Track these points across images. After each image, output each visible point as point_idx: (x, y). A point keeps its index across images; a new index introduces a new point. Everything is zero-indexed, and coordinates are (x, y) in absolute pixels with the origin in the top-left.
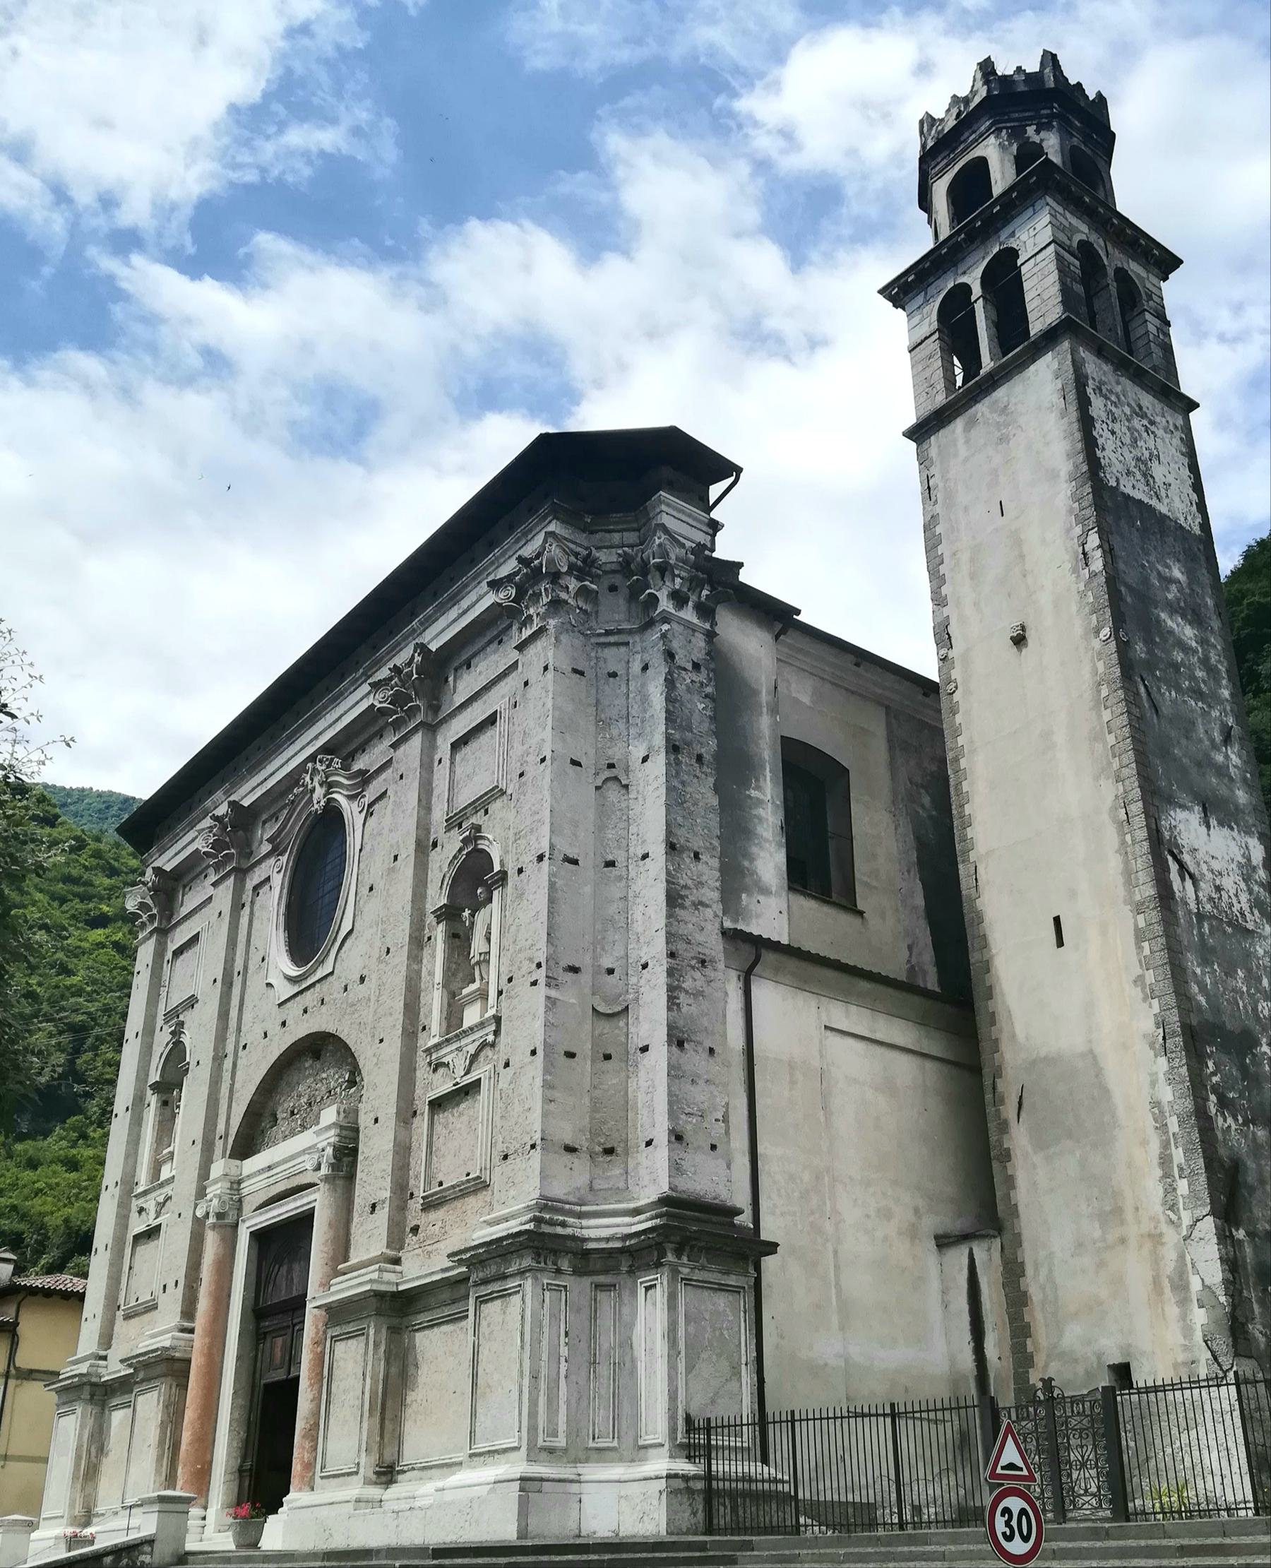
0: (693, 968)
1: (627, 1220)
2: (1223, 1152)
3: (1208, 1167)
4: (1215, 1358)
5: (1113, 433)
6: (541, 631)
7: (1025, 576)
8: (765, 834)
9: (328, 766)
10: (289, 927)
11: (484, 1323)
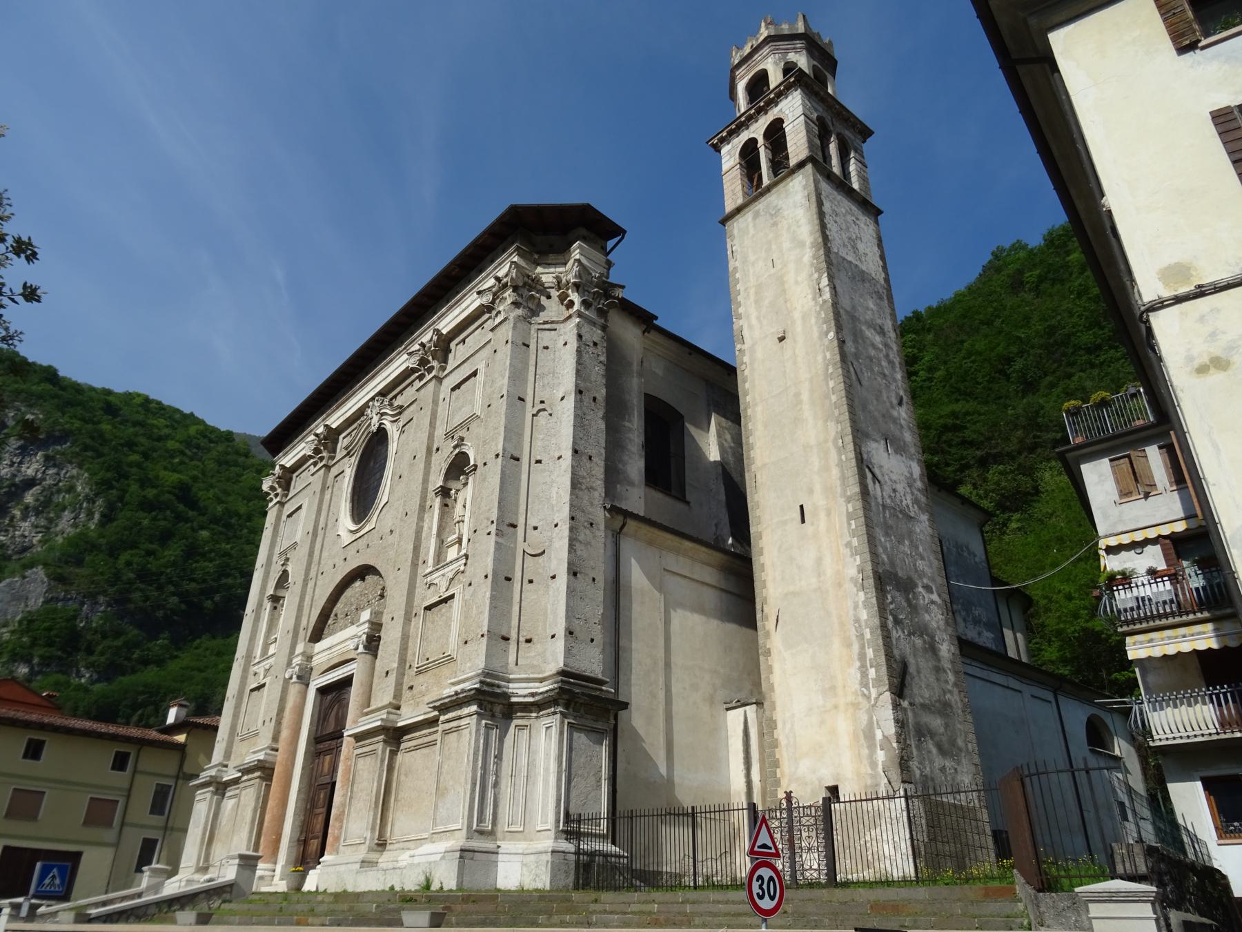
0: (585, 527)
1: (537, 684)
2: (896, 652)
3: (888, 661)
4: (890, 783)
5: (836, 222)
6: (505, 319)
7: (786, 302)
8: (633, 449)
9: (382, 403)
10: (353, 501)
11: (446, 748)
